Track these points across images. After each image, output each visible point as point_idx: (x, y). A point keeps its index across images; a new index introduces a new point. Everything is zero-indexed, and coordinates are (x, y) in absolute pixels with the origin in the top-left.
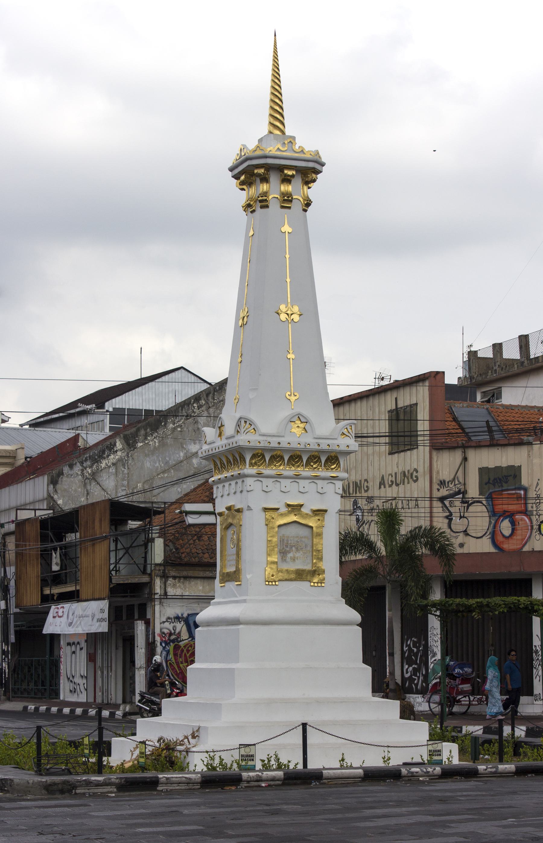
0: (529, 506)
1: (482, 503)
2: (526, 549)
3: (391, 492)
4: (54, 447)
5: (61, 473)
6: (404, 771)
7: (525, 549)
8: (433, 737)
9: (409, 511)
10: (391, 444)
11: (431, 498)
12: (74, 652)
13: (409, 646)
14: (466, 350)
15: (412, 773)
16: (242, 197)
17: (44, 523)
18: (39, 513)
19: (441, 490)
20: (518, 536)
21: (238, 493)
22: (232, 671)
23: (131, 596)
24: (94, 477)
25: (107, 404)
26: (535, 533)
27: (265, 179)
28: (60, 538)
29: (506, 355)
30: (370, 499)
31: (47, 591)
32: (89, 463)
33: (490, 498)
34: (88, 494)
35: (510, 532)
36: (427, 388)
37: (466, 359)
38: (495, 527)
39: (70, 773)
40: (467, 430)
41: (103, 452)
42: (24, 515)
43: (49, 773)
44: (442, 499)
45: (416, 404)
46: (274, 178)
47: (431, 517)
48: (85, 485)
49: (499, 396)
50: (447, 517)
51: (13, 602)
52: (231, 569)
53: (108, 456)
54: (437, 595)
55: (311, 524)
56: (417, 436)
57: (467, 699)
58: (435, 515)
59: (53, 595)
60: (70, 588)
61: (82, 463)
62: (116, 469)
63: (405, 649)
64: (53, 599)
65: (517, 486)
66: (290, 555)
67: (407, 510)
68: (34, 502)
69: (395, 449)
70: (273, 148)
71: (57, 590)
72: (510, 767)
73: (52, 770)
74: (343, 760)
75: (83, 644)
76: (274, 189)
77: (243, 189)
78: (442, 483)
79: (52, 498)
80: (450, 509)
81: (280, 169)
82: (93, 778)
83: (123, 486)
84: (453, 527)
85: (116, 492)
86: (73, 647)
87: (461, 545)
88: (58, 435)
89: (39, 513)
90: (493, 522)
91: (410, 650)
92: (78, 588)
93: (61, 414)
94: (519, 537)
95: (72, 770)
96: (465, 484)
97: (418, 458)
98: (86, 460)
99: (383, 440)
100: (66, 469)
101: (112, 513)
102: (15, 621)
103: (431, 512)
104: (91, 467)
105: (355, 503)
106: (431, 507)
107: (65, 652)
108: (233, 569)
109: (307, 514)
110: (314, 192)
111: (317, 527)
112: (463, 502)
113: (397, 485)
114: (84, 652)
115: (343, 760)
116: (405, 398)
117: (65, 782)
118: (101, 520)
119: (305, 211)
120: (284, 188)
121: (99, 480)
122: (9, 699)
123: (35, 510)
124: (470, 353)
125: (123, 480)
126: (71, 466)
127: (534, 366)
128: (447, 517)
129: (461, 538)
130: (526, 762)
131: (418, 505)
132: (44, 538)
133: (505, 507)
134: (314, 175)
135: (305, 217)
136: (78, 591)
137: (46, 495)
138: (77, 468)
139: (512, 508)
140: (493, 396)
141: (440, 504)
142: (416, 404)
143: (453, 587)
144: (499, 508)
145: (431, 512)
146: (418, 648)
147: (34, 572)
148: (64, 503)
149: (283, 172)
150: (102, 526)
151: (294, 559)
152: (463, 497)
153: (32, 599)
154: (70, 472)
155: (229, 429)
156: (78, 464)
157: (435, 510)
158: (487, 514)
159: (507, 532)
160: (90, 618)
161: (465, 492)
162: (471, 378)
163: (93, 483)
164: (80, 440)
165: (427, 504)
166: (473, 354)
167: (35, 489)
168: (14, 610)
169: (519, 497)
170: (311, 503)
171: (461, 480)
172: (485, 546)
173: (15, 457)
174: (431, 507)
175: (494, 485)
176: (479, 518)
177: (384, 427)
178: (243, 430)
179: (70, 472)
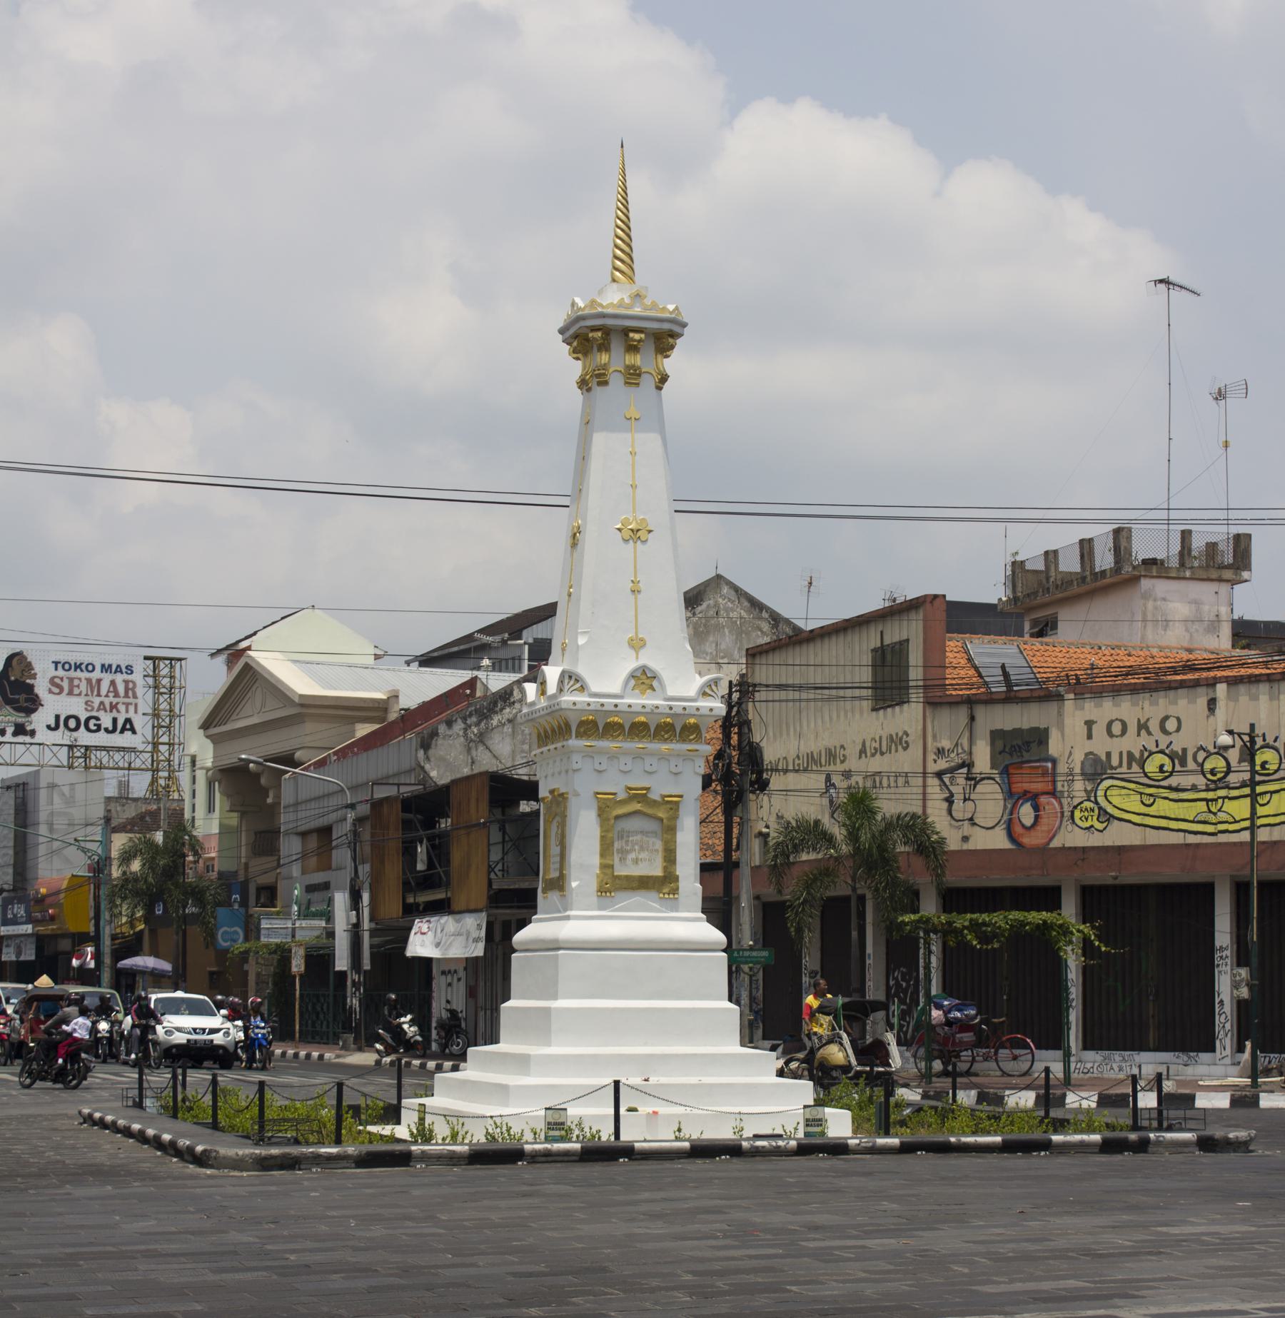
0: (1059, 785)
1: (993, 779)
2: (1056, 843)
3: (876, 764)
4: (441, 696)
5: (434, 734)
6: (745, 1144)
7: (1052, 845)
8: (819, 1103)
9: (897, 791)
10: (876, 699)
11: (924, 773)
12: (450, 985)
13: (895, 979)
14: (1010, 559)
15: (757, 1147)
16: (576, 368)
17: (408, 804)
18: (403, 789)
19: (939, 761)
20: (1043, 827)
21: (563, 774)
22: (547, 1010)
23: (519, 907)
24: (482, 739)
25: (525, 633)
26: (1066, 822)
27: (604, 347)
28: (430, 823)
29: (1063, 567)
30: (847, 774)
31: (411, 900)
32: (474, 719)
33: (1005, 772)
34: (473, 762)
35: (1032, 821)
36: (921, 624)
37: (1009, 573)
38: (1011, 813)
39: (297, 1142)
40: (987, 679)
41: (495, 704)
42: (381, 793)
43: (270, 1142)
44: (939, 775)
45: (908, 640)
46: (617, 346)
47: (924, 800)
48: (469, 750)
49: (1054, 627)
50: (947, 800)
51: (366, 913)
52: (554, 874)
53: (502, 710)
54: (930, 907)
55: (660, 815)
56: (908, 688)
57: (970, 1053)
58: (929, 797)
59: (417, 905)
60: (440, 895)
61: (464, 719)
62: (513, 728)
63: (892, 983)
64: (418, 910)
65: (1043, 756)
66: (632, 856)
67: (892, 790)
68: (398, 774)
69: (881, 704)
70: (613, 298)
71: (423, 898)
72: (895, 1141)
73: (274, 1140)
74: (679, 1130)
75: (462, 974)
76: (615, 360)
77: (578, 359)
78: (940, 752)
79: (422, 768)
80: (951, 788)
81: (626, 331)
82: (323, 1150)
83: (523, 751)
84: (954, 814)
85: (513, 760)
86: (449, 977)
87: (965, 839)
88: (446, 679)
89: (403, 789)
90: (1009, 806)
91: (898, 985)
92: (449, 895)
93: (462, 647)
94: (1045, 828)
95: (300, 1138)
96: (971, 753)
97: (908, 717)
98: (470, 715)
99: (865, 693)
100: (442, 729)
101: (493, 790)
102: (371, 936)
103: (924, 794)
104: (477, 724)
105: (828, 778)
106: (925, 786)
107: (439, 983)
108: (556, 874)
109: (655, 801)
110: (670, 365)
111: (669, 819)
112: (968, 779)
113: (882, 754)
114: (462, 984)
115: (679, 1130)
116: (894, 633)
117: (284, 1156)
118: (477, 800)
119: (660, 389)
120: (631, 359)
121: (489, 743)
122: (360, 1049)
123: (399, 785)
124: (1014, 563)
125: (523, 743)
126: (449, 724)
127: (1099, 584)
128: (947, 800)
129: (967, 829)
130: (908, 1135)
131: (907, 782)
132: (407, 825)
133: (1026, 786)
134: (671, 340)
135: (660, 396)
136: (449, 899)
137: (414, 765)
138: (458, 727)
139: (1036, 787)
140: (1047, 625)
141: (936, 781)
142: (908, 640)
143: (954, 899)
144: (1019, 787)
145: (924, 794)
146: (908, 982)
147: (393, 871)
148: (438, 775)
149: (627, 335)
150: (479, 810)
151: (636, 861)
152: (969, 772)
153: (393, 909)
154: (449, 733)
155: (552, 688)
156: (459, 721)
157: (929, 790)
158: (1000, 796)
159: (1028, 821)
160: (464, 937)
161: (970, 765)
162: (1016, 599)
163: (481, 748)
164: (479, 685)
165: (921, 780)
166: (1018, 567)
167: (395, 757)
168: (366, 925)
169: (1045, 773)
170: (661, 787)
171: (966, 748)
172: (998, 840)
173: (386, 710)
174: (925, 786)
175: (1011, 754)
176: (990, 801)
177: (866, 675)
178: (567, 687)
179: (449, 733)
